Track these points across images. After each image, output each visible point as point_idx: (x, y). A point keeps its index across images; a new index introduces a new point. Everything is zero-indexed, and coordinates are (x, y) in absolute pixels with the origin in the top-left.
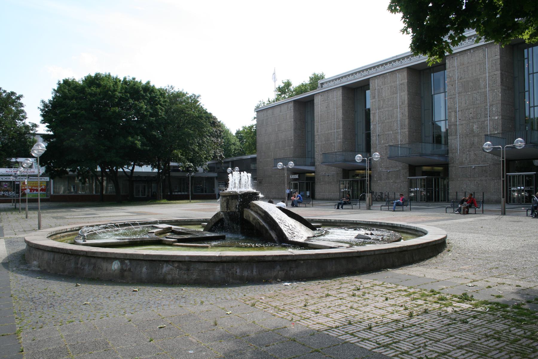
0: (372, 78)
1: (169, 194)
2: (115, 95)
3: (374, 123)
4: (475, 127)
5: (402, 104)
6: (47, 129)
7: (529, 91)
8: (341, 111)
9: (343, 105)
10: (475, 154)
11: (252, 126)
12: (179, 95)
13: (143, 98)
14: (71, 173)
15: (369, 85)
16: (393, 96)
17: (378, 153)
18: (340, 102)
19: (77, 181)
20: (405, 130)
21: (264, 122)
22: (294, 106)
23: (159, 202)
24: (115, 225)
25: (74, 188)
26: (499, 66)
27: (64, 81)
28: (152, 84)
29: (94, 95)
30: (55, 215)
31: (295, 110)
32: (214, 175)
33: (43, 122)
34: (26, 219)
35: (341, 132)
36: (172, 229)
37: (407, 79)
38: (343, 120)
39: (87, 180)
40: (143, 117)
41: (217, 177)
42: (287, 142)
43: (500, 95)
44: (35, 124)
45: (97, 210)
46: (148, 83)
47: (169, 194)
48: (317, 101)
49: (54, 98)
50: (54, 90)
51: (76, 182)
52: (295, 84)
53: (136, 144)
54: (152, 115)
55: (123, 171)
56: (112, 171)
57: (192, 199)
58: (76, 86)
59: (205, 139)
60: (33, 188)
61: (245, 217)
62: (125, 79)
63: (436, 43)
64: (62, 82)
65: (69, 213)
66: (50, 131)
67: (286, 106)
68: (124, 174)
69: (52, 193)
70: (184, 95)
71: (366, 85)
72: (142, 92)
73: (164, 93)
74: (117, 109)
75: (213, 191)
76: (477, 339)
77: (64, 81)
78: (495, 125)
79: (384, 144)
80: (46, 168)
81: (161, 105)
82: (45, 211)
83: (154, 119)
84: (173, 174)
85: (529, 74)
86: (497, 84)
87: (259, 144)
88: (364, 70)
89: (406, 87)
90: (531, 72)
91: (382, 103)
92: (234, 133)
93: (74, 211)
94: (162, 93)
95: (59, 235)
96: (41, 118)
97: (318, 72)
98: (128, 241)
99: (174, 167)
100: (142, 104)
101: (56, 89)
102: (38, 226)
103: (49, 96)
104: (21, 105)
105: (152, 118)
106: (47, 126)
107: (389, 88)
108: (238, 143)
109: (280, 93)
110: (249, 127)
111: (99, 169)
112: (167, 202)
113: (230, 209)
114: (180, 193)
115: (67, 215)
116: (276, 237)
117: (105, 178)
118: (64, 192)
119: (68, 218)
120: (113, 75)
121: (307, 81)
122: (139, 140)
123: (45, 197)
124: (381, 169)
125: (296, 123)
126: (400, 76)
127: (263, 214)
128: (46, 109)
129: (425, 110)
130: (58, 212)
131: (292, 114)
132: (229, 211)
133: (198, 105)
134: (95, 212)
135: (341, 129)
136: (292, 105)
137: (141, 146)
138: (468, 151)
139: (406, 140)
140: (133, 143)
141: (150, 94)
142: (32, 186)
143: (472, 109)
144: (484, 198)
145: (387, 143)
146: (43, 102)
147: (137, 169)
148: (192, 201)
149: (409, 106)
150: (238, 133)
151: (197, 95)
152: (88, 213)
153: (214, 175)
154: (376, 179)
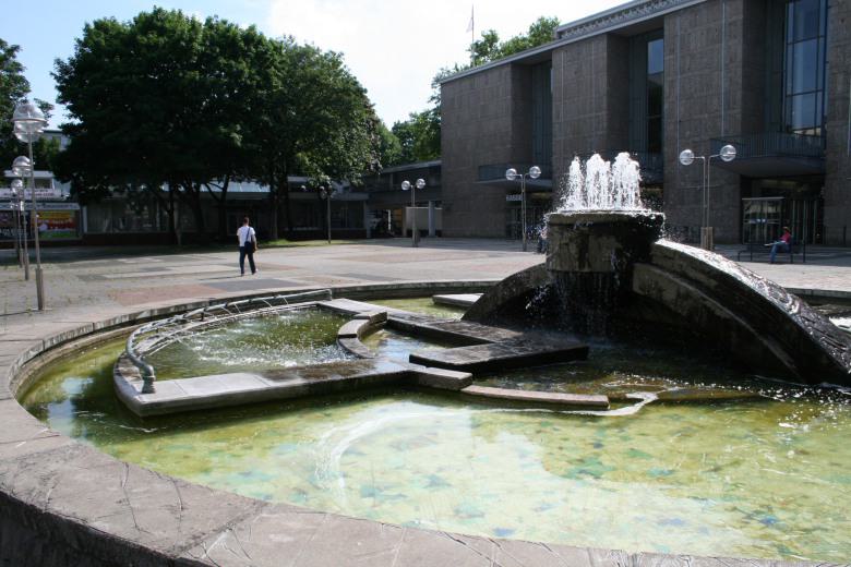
1: (287, 229)
2: (192, 48)
5: (731, 61)
6: (69, 112)
8: (605, 79)
9: (610, 66)
11: (427, 113)
12: (306, 53)
13: (245, 55)
14: (116, 195)
15: (662, 28)
17: (730, 146)
18: (603, 63)
19: (129, 211)
20: (735, 111)
22: (513, 72)
23: (272, 243)
24: (226, 307)
25: (124, 221)
27: (96, 23)
28: (258, 30)
29: (151, 47)
30: (86, 271)
32: (363, 196)
33: (62, 100)
34: (25, 283)
35: (605, 118)
36: (388, 318)
37: (744, 14)
38: (610, 95)
39: (146, 208)
40: (246, 89)
41: (367, 201)
44: (47, 104)
45: (167, 260)
46: (252, 28)
47: (287, 229)
48: (559, 60)
49: (77, 56)
50: (79, 41)
51: (127, 212)
52: (504, 38)
53: (233, 138)
54: (259, 86)
55: (207, 190)
56: (188, 189)
57: (333, 238)
58: (119, 33)
59: (354, 131)
60: (54, 222)
61: (641, 289)
62: (209, 21)
64: (92, 26)
65: (113, 268)
66: (76, 117)
67: (496, 73)
68: (210, 196)
69: (86, 230)
70: (315, 52)
72: (242, 44)
73: (281, 48)
74: (197, 75)
75: (362, 226)
77: (96, 23)
80: (72, 184)
81: (275, 67)
82: (69, 264)
83: (265, 92)
84: (293, 196)
88: (643, 4)
89: (739, 30)
92: (389, 127)
93: (123, 263)
94: (277, 48)
95: (70, 346)
96: (57, 93)
97: (549, 16)
98: (305, 386)
99: (293, 183)
100: (243, 65)
101: (82, 38)
102: (36, 300)
103: (68, 52)
104: (18, 67)
105: (260, 92)
106: (68, 107)
107: (705, 32)
108: (398, 145)
109: (476, 54)
110: (423, 114)
111: (165, 187)
112: (287, 243)
113: (590, 266)
114: (305, 229)
115: (110, 272)
116: (792, 361)
117: (175, 206)
118: (108, 229)
119: (110, 279)
120: (188, 14)
121: (523, 31)
122: (238, 133)
123: (74, 238)
124: (682, 184)
126: (728, 8)
127: (713, 283)
128: (66, 77)
130: (93, 265)
131: (509, 86)
132: (586, 270)
133: (342, 70)
134: (163, 264)
135: (604, 113)
136: (508, 69)
137: (242, 142)
140: (227, 136)
141: (256, 47)
142: (51, 220)
146: (58, 62)
147: (235, 187)
148: (332, 242)
149: (744, 67)
150: (397, 127)
151: (337, 52)
152: (150, 266)
153: (363, 196)
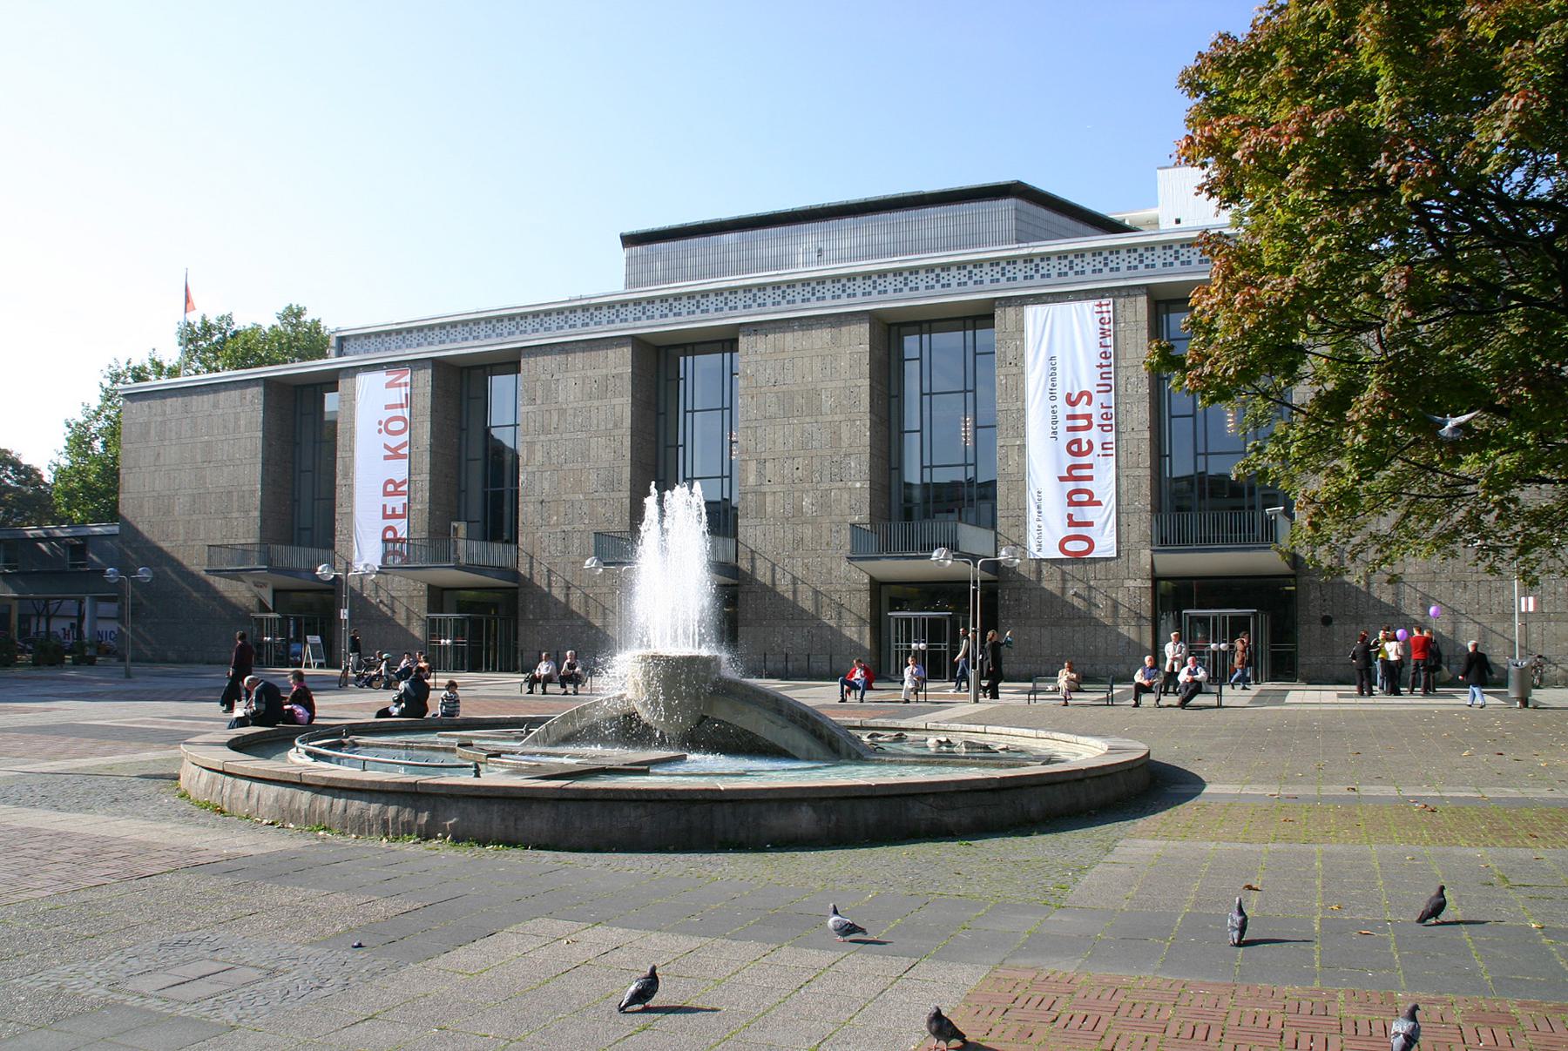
0: (527, 350)
3: (529, 469)
4: (806, 502)
7: (684, 446)
8: (428, 425)
10: (806, 566)
16: (589, 404)
20: (621, 495)
21: (153, 432)
26: (866, 369)
31: (267, 408)
42: (235, 498)
43: (868, 434)
63: (1392, 224)
71: (331, 383)
76: (255, 974)
78: (853, 502)
79: (557, 525)
85: (685, 412)
86: (862, 409)
87: (128, 496)
90: (689, 408)
91: (555, 418)
107: (580, 382)
125: (270, 445)
129: (301, 471)
138: (789, 557)
139: (425, 535)
143: (801, 460)
144: (1496, 636)
145: (569, 524)
154: (531, 617)
